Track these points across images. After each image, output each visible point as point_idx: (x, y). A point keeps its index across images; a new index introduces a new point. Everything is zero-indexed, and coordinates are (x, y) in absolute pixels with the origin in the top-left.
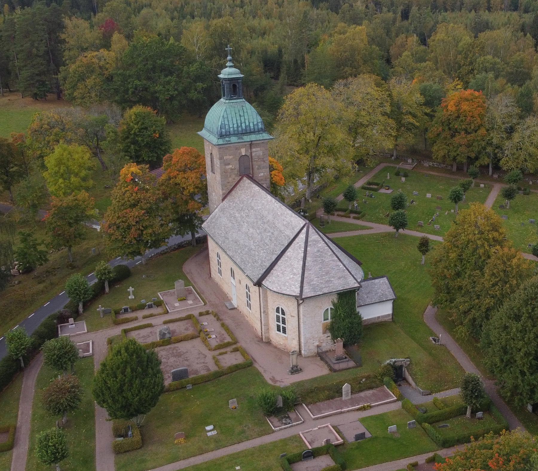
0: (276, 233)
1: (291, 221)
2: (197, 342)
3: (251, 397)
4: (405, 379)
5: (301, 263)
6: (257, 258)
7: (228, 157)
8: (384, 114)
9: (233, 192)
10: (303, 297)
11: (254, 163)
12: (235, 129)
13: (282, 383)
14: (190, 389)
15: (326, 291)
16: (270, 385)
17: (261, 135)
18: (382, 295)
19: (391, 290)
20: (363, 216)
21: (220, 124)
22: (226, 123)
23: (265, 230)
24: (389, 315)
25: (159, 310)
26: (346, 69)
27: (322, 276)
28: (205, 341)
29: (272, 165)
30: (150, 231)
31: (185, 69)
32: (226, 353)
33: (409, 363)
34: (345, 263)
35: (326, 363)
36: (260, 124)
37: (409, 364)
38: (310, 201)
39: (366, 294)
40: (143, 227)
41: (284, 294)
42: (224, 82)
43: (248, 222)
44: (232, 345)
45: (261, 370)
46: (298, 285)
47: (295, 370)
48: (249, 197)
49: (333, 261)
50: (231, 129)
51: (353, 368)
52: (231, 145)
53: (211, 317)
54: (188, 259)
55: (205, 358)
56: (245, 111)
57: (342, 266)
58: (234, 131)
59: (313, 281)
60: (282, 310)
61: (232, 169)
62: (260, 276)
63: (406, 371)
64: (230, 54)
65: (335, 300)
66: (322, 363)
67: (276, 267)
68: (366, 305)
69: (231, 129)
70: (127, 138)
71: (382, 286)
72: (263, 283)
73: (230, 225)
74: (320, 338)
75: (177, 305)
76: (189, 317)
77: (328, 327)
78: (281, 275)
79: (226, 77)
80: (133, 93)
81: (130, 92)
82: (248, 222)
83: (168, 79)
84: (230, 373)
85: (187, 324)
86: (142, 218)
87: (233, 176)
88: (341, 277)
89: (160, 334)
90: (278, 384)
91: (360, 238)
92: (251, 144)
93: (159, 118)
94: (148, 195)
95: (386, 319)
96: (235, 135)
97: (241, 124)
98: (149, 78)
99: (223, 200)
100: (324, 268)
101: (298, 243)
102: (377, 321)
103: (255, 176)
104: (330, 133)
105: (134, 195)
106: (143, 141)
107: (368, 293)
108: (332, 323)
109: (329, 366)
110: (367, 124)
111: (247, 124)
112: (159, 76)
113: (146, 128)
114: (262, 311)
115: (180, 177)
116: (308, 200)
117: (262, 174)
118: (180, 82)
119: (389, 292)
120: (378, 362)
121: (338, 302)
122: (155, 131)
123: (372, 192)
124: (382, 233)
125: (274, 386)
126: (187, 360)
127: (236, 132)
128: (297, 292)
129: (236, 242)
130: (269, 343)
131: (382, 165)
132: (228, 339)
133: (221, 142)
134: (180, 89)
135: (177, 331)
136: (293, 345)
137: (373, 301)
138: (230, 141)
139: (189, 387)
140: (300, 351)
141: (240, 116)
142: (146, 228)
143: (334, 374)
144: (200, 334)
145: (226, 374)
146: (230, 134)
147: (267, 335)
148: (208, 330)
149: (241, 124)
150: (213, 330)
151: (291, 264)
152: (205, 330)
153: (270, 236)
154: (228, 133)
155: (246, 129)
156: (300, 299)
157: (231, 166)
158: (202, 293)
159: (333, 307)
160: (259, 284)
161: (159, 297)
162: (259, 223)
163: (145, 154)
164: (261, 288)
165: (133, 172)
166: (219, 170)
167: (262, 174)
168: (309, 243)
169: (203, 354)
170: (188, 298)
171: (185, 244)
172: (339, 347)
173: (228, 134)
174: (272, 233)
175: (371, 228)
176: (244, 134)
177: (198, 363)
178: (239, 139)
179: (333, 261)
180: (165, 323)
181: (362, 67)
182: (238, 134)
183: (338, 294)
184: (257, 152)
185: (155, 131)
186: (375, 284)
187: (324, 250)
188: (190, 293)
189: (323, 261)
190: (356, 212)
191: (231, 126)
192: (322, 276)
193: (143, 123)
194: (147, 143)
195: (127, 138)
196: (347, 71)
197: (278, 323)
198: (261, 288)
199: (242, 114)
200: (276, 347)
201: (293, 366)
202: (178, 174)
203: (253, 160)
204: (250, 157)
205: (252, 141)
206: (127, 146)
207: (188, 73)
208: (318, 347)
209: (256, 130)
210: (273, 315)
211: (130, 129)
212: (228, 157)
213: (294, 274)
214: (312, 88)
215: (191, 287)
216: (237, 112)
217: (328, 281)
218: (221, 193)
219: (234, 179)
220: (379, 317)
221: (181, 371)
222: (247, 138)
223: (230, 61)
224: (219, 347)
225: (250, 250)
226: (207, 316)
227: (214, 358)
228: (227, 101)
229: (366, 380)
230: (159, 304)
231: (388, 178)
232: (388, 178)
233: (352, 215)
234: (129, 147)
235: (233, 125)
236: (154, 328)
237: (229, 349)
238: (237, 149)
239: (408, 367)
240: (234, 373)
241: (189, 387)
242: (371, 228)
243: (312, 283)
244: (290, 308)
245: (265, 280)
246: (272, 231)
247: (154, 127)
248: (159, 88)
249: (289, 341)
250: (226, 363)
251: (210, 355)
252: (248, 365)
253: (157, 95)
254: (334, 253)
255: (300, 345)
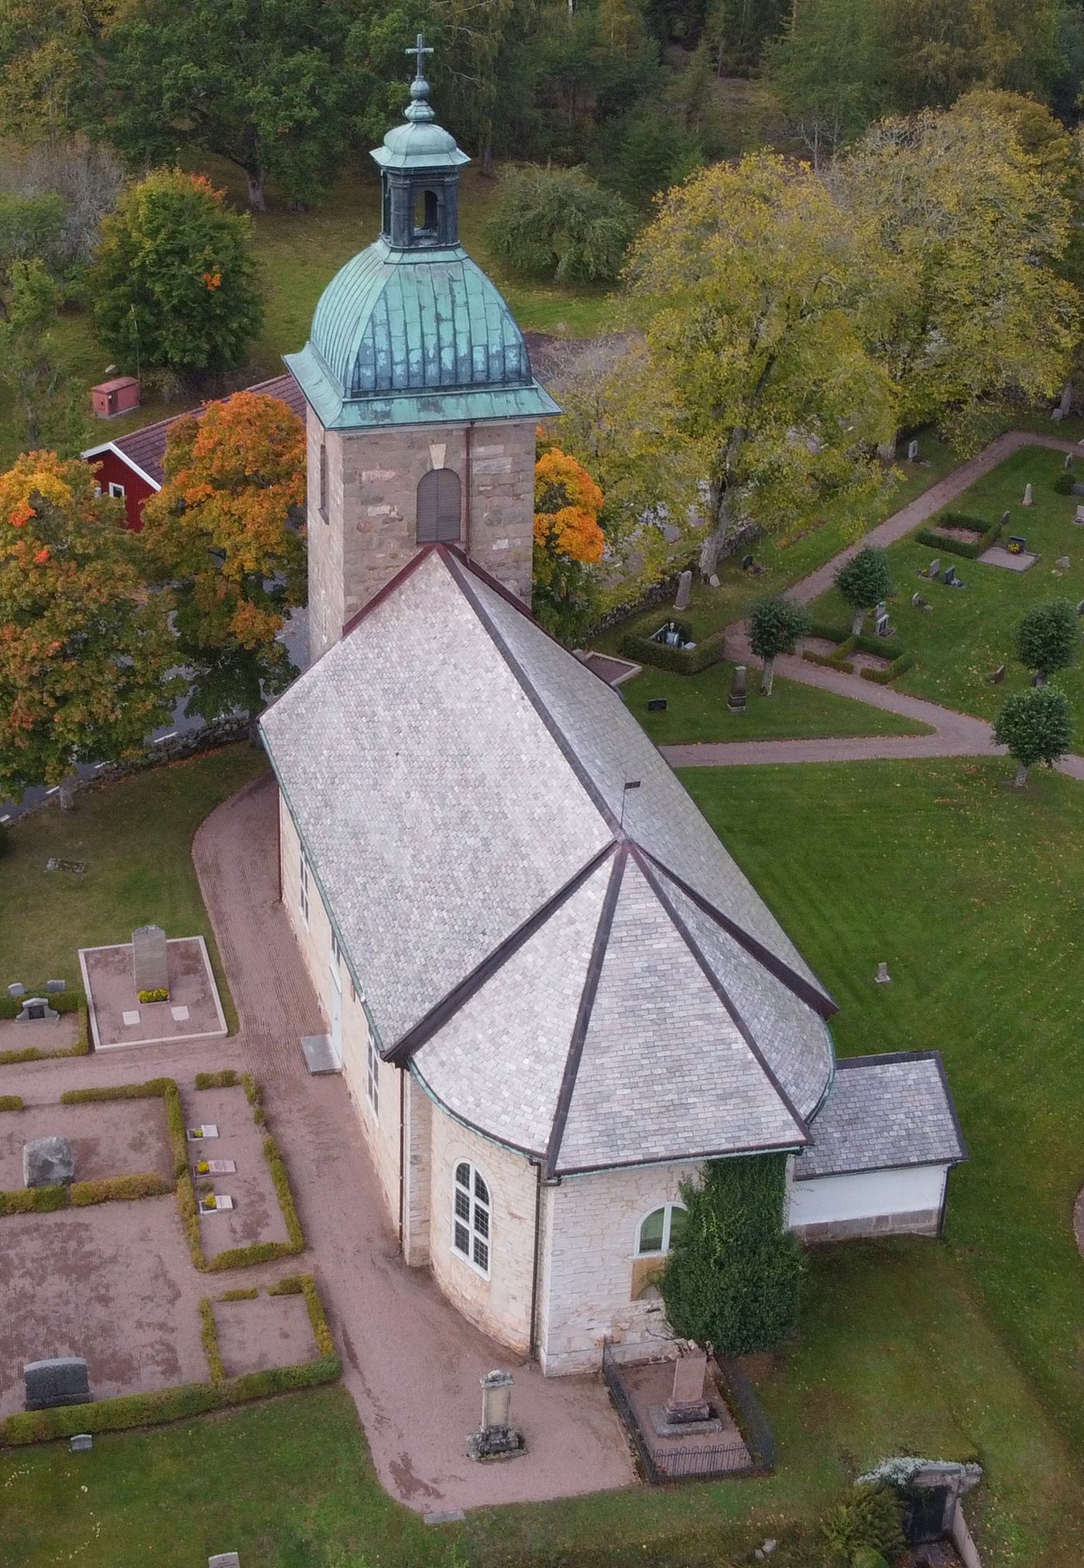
0: (499, 846)
1: (560, 809)
2: (161, 1214)
3: (300, 1546)
4: (948, 1538)
5: (573, 1013)
6: (412, 936)
7: (377, 474)
8: (1042, 258)
9: (386, 606)
10: (560, 1166)
11: (476, 500)
12: (415, 368)
13: (430, 1500)
14: (85, 1452)
15: (662, 1152)
16: (390, 1501)
17: (511, 397)
18: (909, 1137)
19: (946, 1118)
20: (902, 670)
21: (356, 347)
22: (382, 343)
23: (465, 816)
24: (926, 1214)
25: (56, 1033)
26: (930, 47)
27: (650, 1080)
28: (190, 1216)
29: (562, 485)
30: (76, 713)
31: (356, 29)
32: (252, 1295)
33: (975, 1480)
34: (755, 1027)
35: (632, 1423)
36: (512, 355)
37: (977, 1486)
38: (714, 580)
39: (840, 1124)
40: (52, 694)
41: (485, 1134)
42: (391, 180)
43: (410, 758)
44: (279, 1261)
45: (366, 1410)
46: (548, 1107)
47: (500, 1445)
48: (434, 645)
49: (707, 1017)
50: (399, 370)
51: (735, 1474)
52: (394, 430)
53: (236, 1101)
54: (220, 800)
55: (172, 1301)
56: (460, 299)
57: (741, 1044)
58: (409, 375)
59: (608, 1099)
60: (478, 1179)
61: (387, 520)
62: (409, 1026)
63: (959, 1511)
64: (425, 72)
65: (695, 1178)
66: (610, 1423)
67: (473, 1005)
68: (834, 1174)
69: (399, 370)
70: (120, 278)
71: (912, 1094)
72: (418, 1056)
73: (350, 748)
74: (619, 1311)
75: (131, 1018)
76: (157, 1090)
77: (655, 1277)
78: (486, 1048)
79: (399, 162)
80: (177, 104)
81: (166, 103)
82: (410, 758)
83: (292, 62)
84: (246, 1402)
85: (146, 1117)
86: (50, 666)
87: (393, 545)
88: (731, 1095)
89: (30, 1164)
90: (417, 1503)
91: (874, 773)
92: (471, 431)
93: (231, 218)
94: (84, 579)
95: (913, 1227)
96: (409, 390)
97: (439, 349)
98: (230, 56)
99: (348, 629)
100: (665, 1048)
101: (572, 922)
102: (874, 1232)
103: (476, 548)
104: (812, 345)
105: (33, 577)
106: (168, 294)
107: (851, 1122)
108: (674, 1266)
109: (639, 1443)
110: (968, 299)
111: (463, 350)
112: (267, 52)
113: (182, 253)
114: (408, 1154)
115: (216, 506)
116: (706, 578)
117: (504, 544)
118: (334, 73)
119: (938, 1125)
120: (846, 1457)
121: (708, 1185)
122: (209, 266)
123: (956, 562)
124: (965, 759)
125: (401, 1512)
126: (105, 1300)
127: (416, 382)
128: (538, 1138)
129: (355, 835)
130: (424, 1273)
131: (1016, 440)
132: (275, 1232)
133: (353, 416)
134: (330, 99)
135: (103, 1149)
136: (509, 1322)
137: (866, 1161)
138: (387, 414)
139: (83, 1441)
140: (534, 1347)
141: (439, 319)
142: (63, 700)
143: (653, 1494)
144: (184, 1177)
145: (229, 1405)
146: (392, 389)
147: (420, 1242)
148: (212, 1165)
149: (439, 349)
150: (231, 1169)
151: (531, 1010)
152: (201, 1167)
153: (475, 851)
154: (385, 385)
155: (455, 374)
156: (548, 1170)
157: (384, 509)
158: (234, 977)
159: (682, 1206)
160: (401, 1056)
161: (74, 975)
162: (450, 776)
163: (174, 342)
164: (407, 1074)
165: (36, 494)
166: (340, 520)
167: (507, 543)
168: (615, 933)
169: (171, 1284)
170: (179, 993)
171: (227, 734)
172: (693, 1375)
173: (385, 389)
174: (486, 842)
175: (925, 730)
176: (445, 388)
177: (140, 1325)
178: (424, 407)
179: (707, 1017)
180: (72, 1100)
181: (988, 44)
182: (424, 388)
183: (712, 1164)
184: (494, 459)
185: (209, 266)
186: (884, 1086)
187: (676, 966)
188: (189, 970)
189: (663, 1018)
190: (877, 652)
191: (399, 356)
192: (650, 1080)
193: (172, 237)
194: (181, 301)
195: (120, 278)
196: (930, 56)
197: (462, 1222)
198: (407, 1074)
199: (445, 312)
200: (445, 1302)
201: (489, 1427)
202: (209, 496)
203: (474, 490)
204: (462, 476)
205: (472, 421)
206: (116, 308)
207: (364, 45)
208: (607, 1343)
209: (496, 375)
210: (444, 1188)
211: (129, 250)
212: (377, 474)
213: (538, 1057)
214: (762, 167)
215: (201, 939)
216: (428, 301)
217: (671, 1108)
218: (342, 606)
219: (394, 556)
220: (882, 1220)
221: (62, 1372)
222: (455, 408)
223: (420, 98)
224: (236, 1262)
225: (396, 888)
226: (225, 1095)
227: (205, 1311)
228: (396, 257)
229: (779, 1547)
230: (68, 1004)
231: (1027, 501)
232: (1027, 501)
233: (862, 662)
234: (125, 311)
235: (408, 351)
236: (28, 1116)
237: (267, 1278)
238: (417, 444)
239: (971, 1498)
240: (262, 1405)
241: (83, 1441)
242: (925, 730)
243: (605, 1108)
244: (511, 1189)
245: (426, 1047)
246: (485, 831)
247: (208, 249)
248: (259, 93)
249: (492, 1294)
250: (242, 1345)
251: (197, 1287)
252: (317, 1388)
253: (253, 117)
254: (716, 985)
255: (535, 1326)
